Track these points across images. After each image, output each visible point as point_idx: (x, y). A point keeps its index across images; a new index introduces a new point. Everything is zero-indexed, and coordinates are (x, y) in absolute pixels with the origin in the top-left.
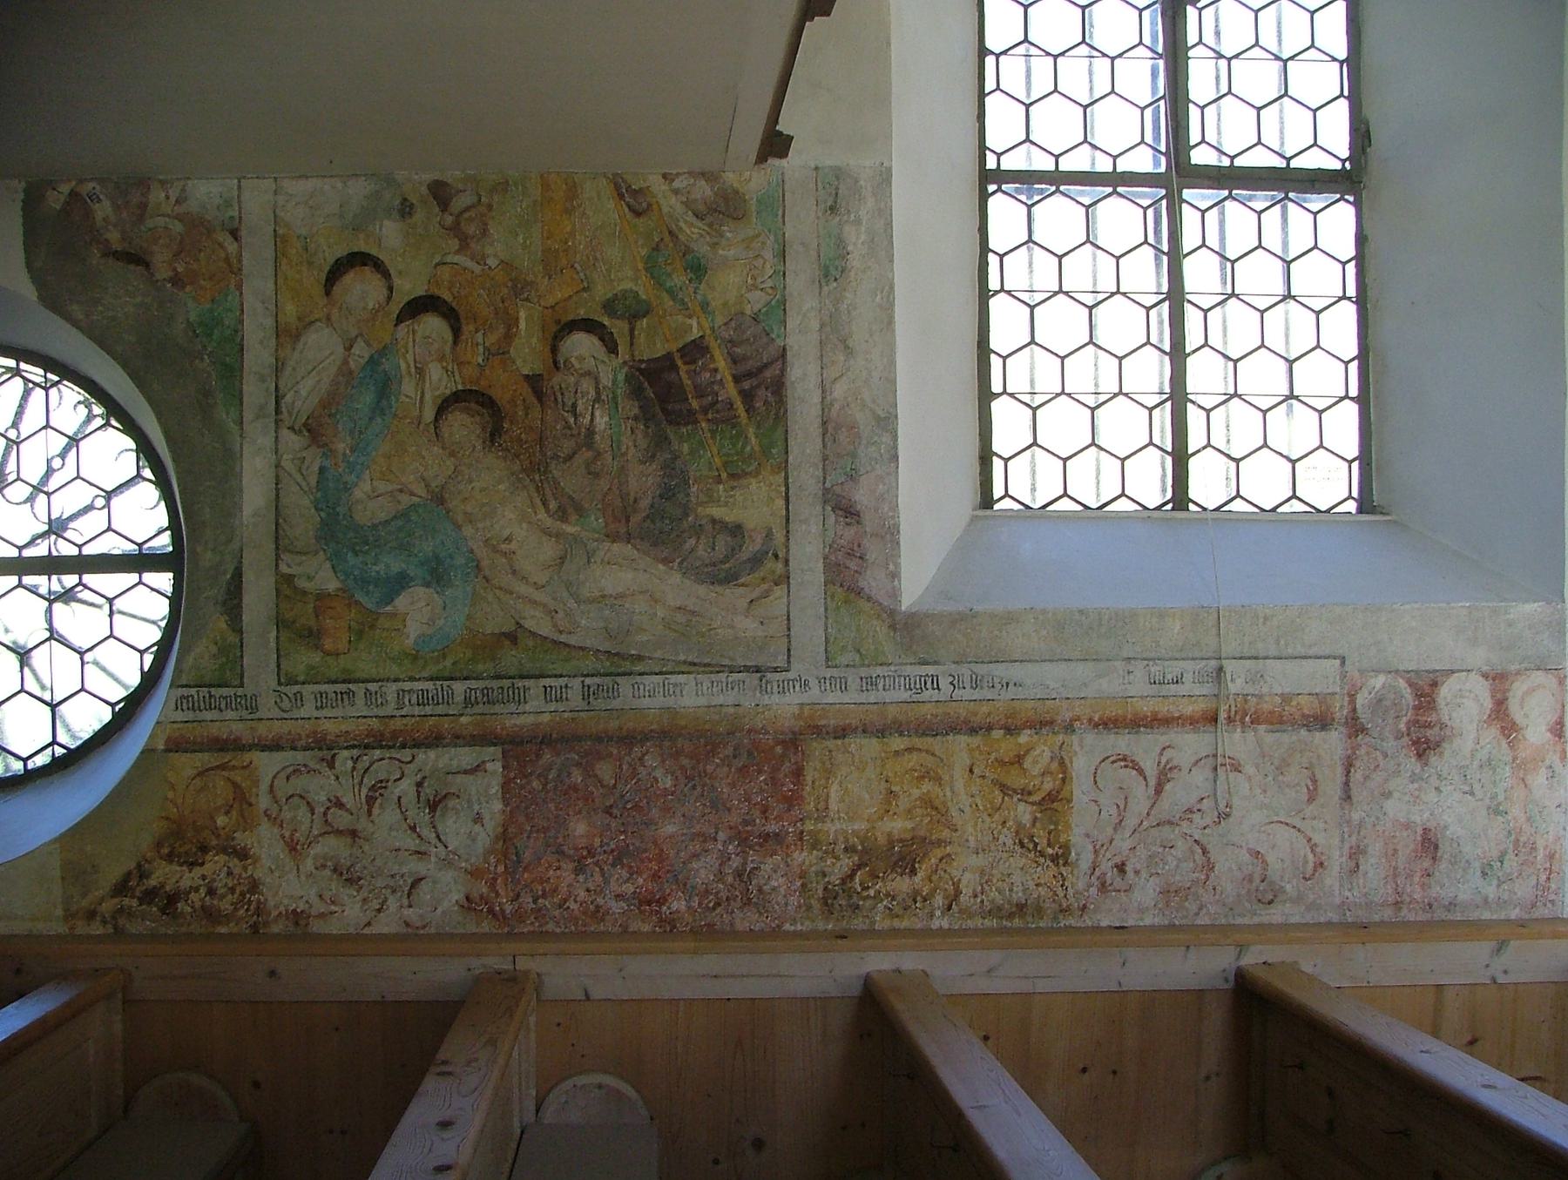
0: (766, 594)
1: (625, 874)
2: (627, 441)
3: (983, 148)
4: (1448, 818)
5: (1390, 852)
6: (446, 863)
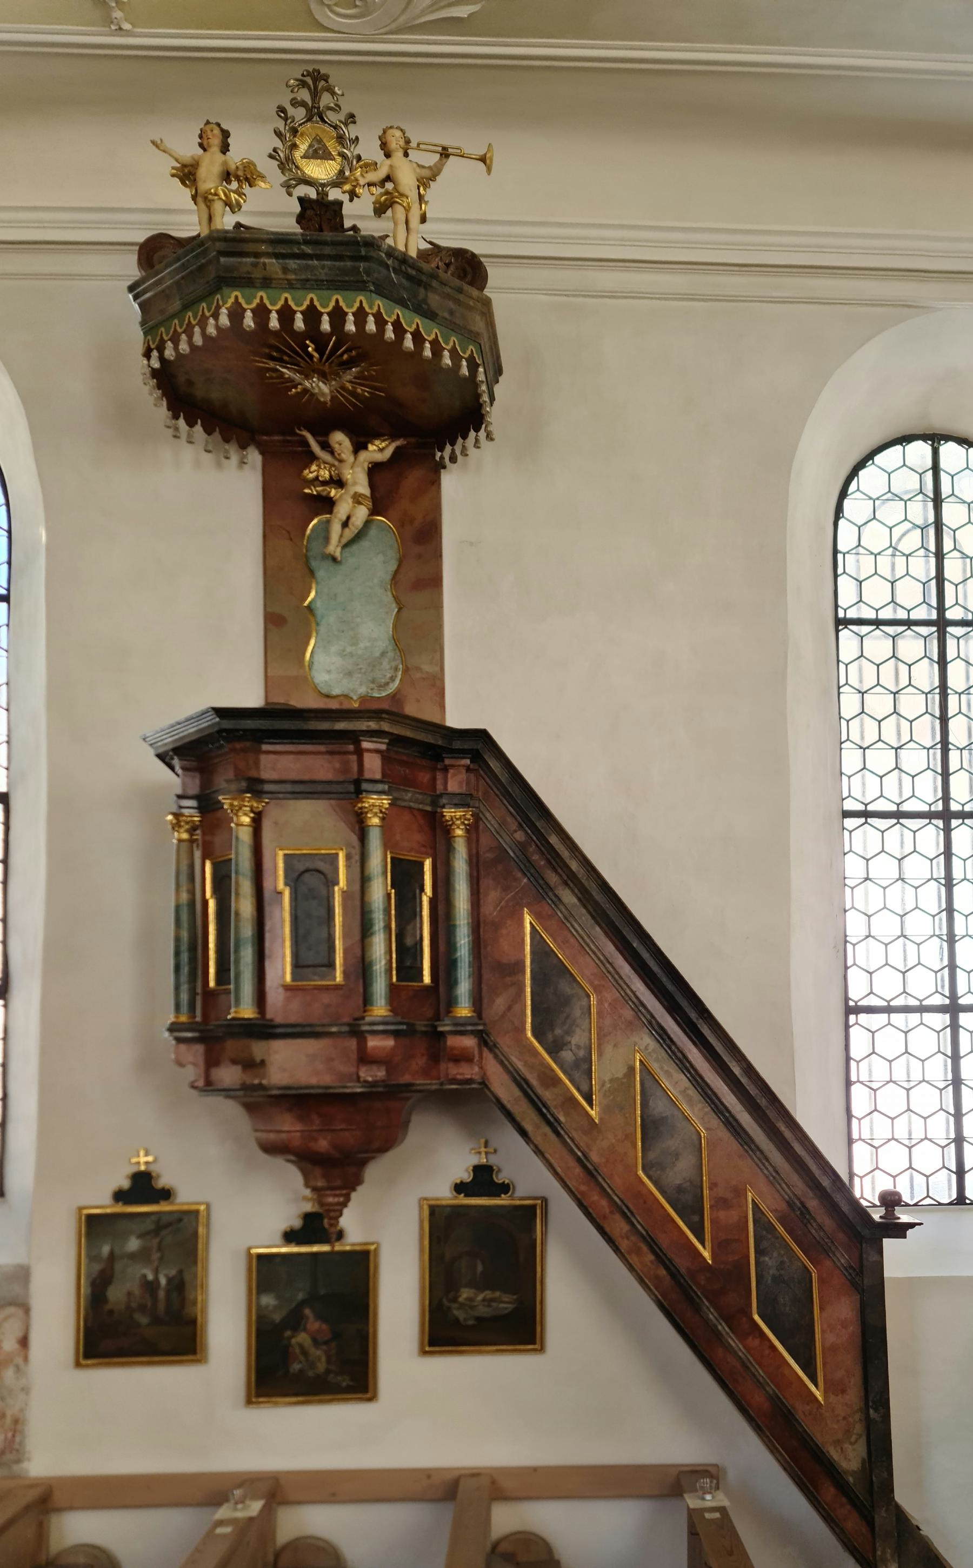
3: (836, 606)
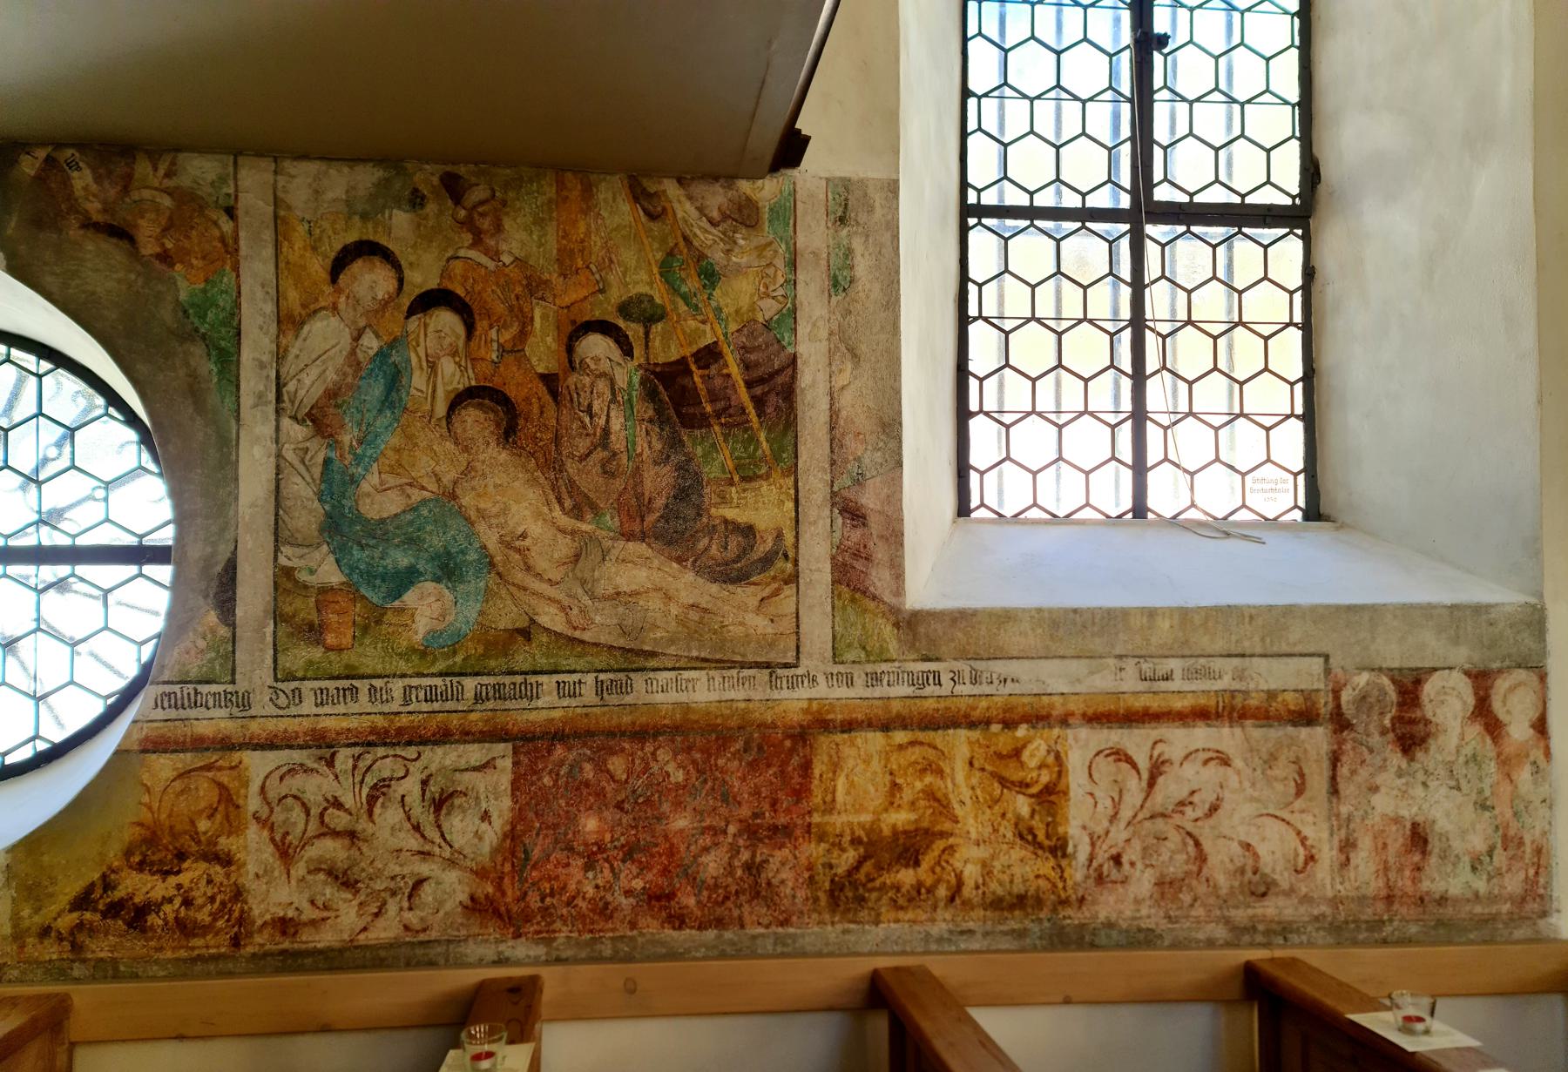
0: (776, 593)
1: (635, 870)
2: (641, 445)
3: (964, 185)
4: (1437, 813)
5: (1380, 845)
6: (451, 863)
